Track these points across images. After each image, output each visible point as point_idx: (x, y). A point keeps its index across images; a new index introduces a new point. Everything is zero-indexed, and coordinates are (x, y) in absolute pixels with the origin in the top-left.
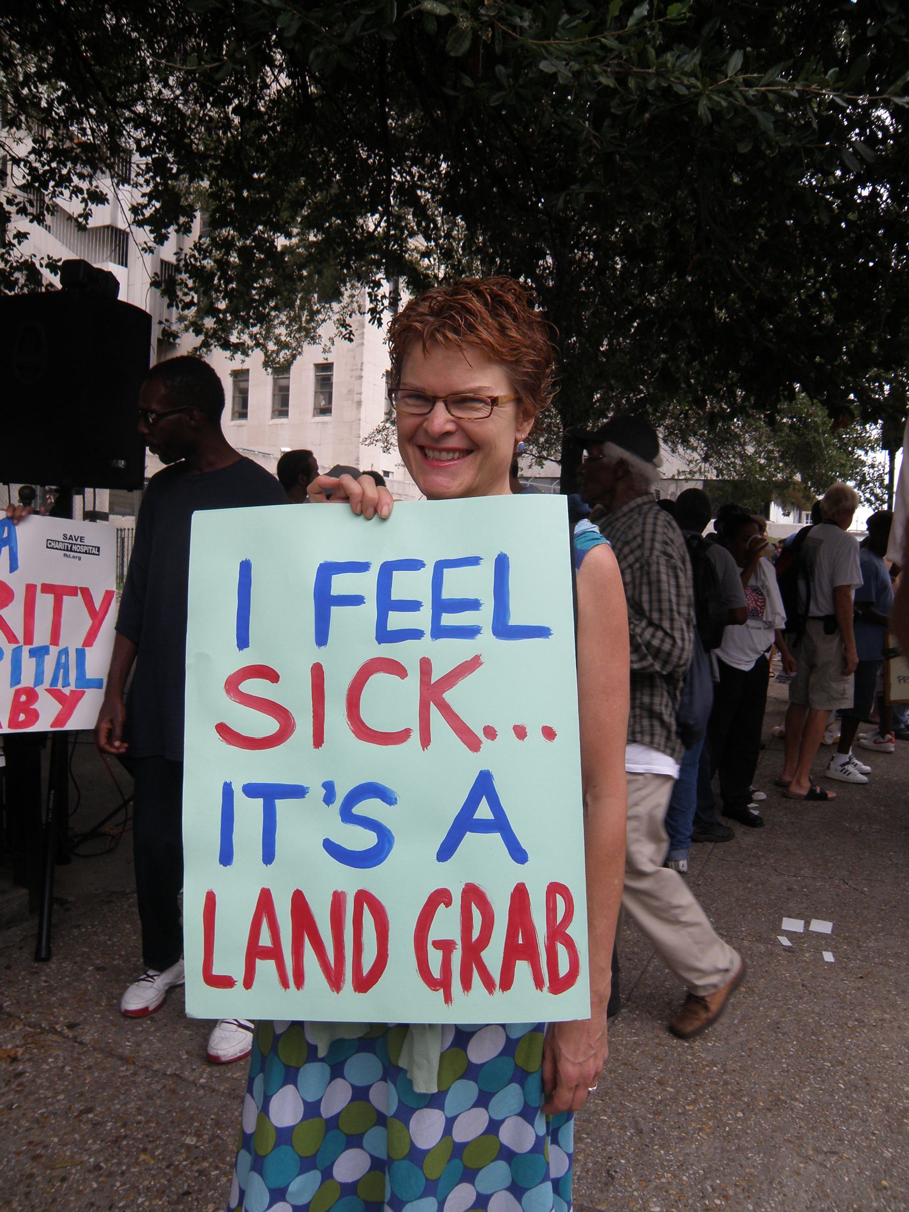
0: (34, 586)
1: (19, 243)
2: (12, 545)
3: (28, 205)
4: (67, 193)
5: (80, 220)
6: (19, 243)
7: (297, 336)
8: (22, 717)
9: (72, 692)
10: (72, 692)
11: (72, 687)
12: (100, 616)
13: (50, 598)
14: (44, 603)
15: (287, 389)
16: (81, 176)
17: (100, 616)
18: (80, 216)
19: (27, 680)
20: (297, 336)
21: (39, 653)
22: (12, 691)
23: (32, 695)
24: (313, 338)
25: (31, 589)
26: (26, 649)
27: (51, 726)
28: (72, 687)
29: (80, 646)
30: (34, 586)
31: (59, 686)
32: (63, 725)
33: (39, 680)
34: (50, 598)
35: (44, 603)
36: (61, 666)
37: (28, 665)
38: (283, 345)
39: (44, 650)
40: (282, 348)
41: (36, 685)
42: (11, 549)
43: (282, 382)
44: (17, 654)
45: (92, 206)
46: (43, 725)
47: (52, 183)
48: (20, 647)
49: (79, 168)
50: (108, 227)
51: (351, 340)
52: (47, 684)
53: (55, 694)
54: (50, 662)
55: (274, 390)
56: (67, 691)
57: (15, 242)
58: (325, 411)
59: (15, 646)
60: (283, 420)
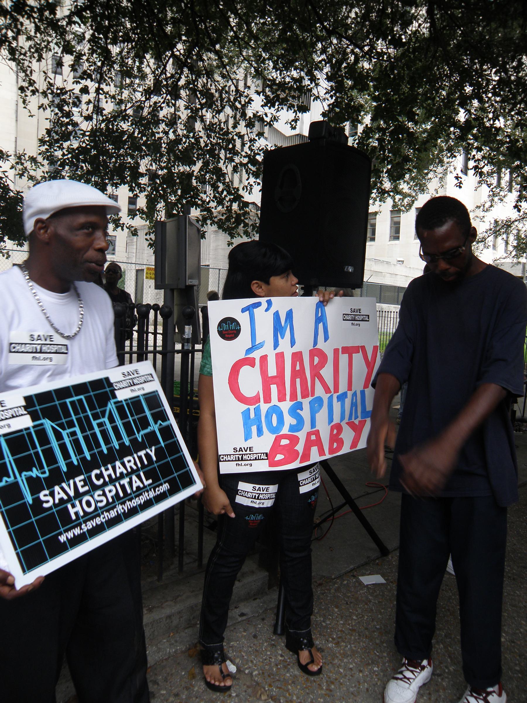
0: (338, 349)
1: (259, 139)
2: (324, 321)
3: (264, 116)
4: (285, 108)
5: (292, 123)
6: (259, 139)
7: (415, 188)
8: (335, 445)
9: (359, 421)
10: (359, 421)
11: (360, 419)
12: (372, 365)
13: (346, 356)
14: (344, 359)
15: (399, 223)
16: (294, 97)
17: (372, 365)
18: (293, 121)
19: (336, 419)
20: (415, 188)
21: (342, 398)
22: (329, 428)
23: (339, 428)
24: (423, 190)
25: (336, 351)
26: (335, 396)
27: (351, 449)
28: (360, 419)
29: (362, 389)
30: (338, 349)
31: (353, 420)
32: (356, 447)
33: (342, 418)
34: (346, 356)
35: (344, 359)
36: (354, 405)
37: (337, 406)
38: (405, 195)
39: (345, 395)
40: (405, 197)
41: (341, 421)
42: (324, 324)
43: (396, 219)
44: (330, 399)
45: (299, 114)
46: (346, 450)
47: (277, 104)
48: (332, 396)
49: (292, 93)
50: (298, 135)
51: (460, 187)
52: (346, 420)
53: (351, 424)
54: (348, 401)
55: (391, 224)
56: (357, 422)
57: (257, 138)
58: (398, 238)
59: (329, 395)
60: (396, 242)
